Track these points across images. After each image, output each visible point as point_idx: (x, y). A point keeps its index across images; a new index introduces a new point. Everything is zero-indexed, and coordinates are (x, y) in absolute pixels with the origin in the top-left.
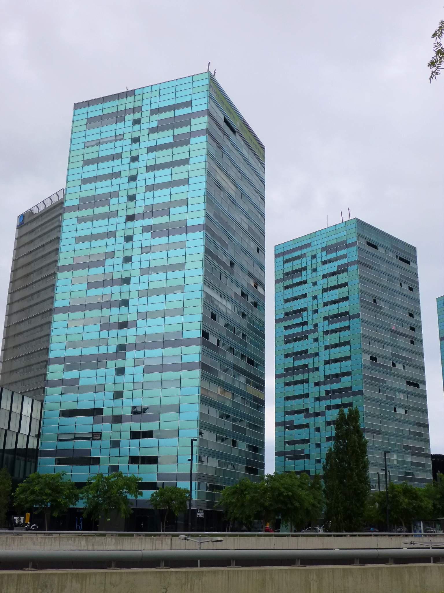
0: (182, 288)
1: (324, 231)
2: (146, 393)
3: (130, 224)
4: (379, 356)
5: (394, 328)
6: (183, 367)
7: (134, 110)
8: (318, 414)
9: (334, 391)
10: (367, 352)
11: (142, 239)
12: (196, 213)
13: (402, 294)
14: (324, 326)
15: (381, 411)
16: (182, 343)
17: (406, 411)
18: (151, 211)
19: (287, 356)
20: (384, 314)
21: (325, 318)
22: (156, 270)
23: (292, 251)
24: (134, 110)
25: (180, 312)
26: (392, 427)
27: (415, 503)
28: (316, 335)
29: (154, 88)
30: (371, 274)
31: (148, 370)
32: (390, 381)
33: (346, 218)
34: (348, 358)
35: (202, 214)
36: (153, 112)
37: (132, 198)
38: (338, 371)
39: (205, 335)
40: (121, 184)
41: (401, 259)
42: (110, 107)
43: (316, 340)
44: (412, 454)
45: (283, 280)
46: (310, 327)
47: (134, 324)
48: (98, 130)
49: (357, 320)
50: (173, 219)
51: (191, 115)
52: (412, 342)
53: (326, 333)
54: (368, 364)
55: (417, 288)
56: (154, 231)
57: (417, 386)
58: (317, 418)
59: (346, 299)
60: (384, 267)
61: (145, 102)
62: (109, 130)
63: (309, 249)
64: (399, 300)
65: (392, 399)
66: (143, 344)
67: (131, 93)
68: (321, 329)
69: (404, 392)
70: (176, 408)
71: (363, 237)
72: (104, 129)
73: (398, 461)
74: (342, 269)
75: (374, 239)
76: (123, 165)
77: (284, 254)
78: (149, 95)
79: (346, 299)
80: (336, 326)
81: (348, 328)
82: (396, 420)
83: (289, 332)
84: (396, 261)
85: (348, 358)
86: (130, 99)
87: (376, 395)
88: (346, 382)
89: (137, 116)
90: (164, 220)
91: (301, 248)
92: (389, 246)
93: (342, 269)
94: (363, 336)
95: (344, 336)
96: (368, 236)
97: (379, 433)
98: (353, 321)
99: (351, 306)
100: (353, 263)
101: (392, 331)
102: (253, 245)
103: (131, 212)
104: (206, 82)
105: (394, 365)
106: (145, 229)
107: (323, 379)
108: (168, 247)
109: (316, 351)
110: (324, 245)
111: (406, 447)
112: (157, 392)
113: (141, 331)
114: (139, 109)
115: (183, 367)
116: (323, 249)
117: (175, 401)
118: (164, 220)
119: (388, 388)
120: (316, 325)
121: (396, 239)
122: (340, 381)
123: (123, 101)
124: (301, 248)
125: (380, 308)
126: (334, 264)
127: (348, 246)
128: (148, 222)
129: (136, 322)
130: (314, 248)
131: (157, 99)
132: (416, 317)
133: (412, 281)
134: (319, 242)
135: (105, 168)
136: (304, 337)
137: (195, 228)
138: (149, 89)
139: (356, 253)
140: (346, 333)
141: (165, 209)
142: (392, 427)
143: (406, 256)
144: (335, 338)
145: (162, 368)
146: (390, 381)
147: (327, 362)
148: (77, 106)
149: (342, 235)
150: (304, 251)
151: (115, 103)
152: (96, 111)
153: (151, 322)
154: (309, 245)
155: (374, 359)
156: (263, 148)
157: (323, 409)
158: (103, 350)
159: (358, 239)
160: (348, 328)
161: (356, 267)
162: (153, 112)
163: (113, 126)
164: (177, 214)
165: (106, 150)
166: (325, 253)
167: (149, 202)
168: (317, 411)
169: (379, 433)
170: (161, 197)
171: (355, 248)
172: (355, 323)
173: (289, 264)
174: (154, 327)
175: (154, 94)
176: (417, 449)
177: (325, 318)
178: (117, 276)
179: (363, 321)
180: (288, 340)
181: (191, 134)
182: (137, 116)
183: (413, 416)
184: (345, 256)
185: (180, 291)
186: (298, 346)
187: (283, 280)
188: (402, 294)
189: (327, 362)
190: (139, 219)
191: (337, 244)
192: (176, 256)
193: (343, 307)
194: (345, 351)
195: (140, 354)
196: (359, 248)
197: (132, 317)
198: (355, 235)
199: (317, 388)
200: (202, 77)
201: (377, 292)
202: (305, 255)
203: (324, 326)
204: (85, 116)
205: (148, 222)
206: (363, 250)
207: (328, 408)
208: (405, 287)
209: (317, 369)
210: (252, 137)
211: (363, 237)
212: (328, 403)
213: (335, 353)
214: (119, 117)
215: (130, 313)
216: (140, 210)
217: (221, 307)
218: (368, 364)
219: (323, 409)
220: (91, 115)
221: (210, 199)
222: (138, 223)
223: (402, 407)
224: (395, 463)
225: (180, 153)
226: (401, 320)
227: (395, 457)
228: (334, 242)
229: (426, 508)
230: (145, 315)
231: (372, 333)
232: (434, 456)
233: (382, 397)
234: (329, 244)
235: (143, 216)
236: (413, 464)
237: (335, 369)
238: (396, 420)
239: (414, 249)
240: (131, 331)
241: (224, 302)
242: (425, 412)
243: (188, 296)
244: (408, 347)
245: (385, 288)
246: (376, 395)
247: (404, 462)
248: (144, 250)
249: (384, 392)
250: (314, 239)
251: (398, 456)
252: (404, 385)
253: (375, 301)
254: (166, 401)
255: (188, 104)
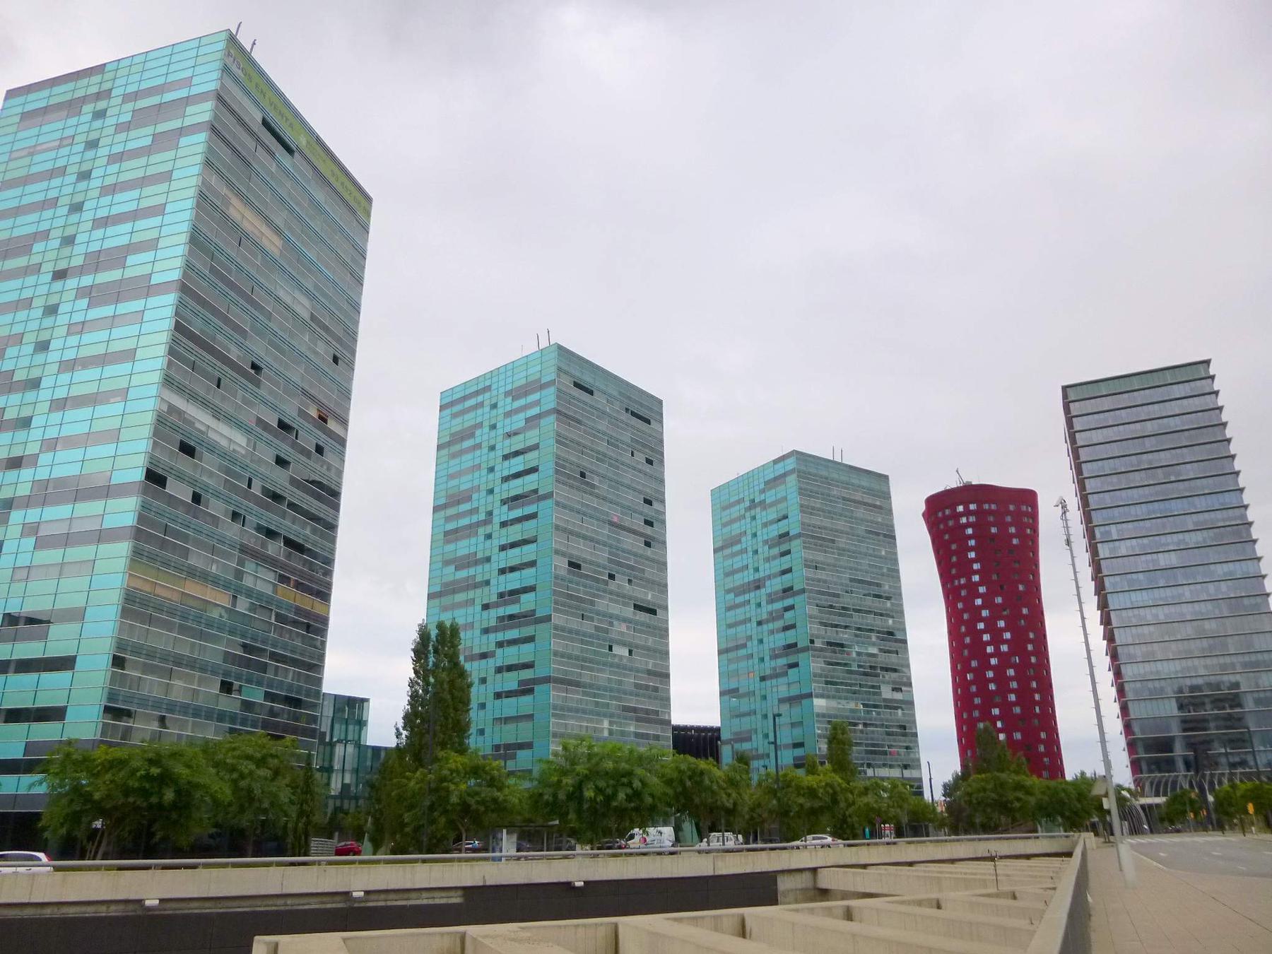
0: (123, 394)
1: (510, 367)
2: (33, 586)
3: (58, 285)
4: (585, 561)
5: (615, 520)
6: (103, 536)
7: (98, 96)
8: (484, 656)
9: (511, 617)
10: (564, 554)
11: (74, 309)
12: (169, 263)
13: (634, 469)
14: (502, 514)
15: (582, 650)
16: (107, 491)
17: (630, 652)
18: (96, 262)
19: (447, 563)
20: (597, 496)
21: (504, 502)
22: (86, 363)
23: (465, 398)
24: (98, 96)
25: (114, 436)
26: (604, 676)
27: (487, 793)
28: (488, 529)
29: (136, 60)
30: (573, 433)
31: (43, 543)
32: (603, 604)
33: (544, 344)
34: (532, 564)
35: (179, 263)
36: (127, 98)
37: (69, 241)
38: (517, 586)
39: (155, 478)
40: (55, 221)
41: (633, 414)
42: (62, 94)
43: (489, 536)
44: (638, 720)
45: (449, 444)
46: (482, 517)
47: (33, 460)
48: (35, 131)
49: (549, 502)
50: (129, 273)
51: (188, 101)
52: (648, 544)
53: (504, 524)
54: (563, 573)
55: (662, 462)
56: (94, 296)
57: (653, 612)
58: (484, 662)
59: (534, 470)
60: (603, 425)
61: (118, 82)
62: (53, 129)
63: (487, 395)
64: (628, 477)
65: (607, 631)
66: (46, 493)
67: (100, 69)
68: (496, 520)
69: (625, 620)
70: (77, 615)
71: (566, 373)
72: (45, 128)
73: (611, 732)
74: (532, 422)
75: (587, 379)
76: (64, 187)
77: (452, 404)
78: (126, 72)
79: (534, 470)
80: (517, 513)
81: (533, 516)
82: (612, 665)
83: (451, 526)
84: (625, 417)
85: (532, 564)
86: (96, 79)
87: (575, 623)
88: (527, 602)
89: (101, 105)
90: (115, 275)
91: (477, 393)
92: (615, 393)
93: (532, 422)
94: (557, 528)
95: (529, 528)
96: (578, 374)
97: (578, 684)
98: (542, 504)
99: (542, 481)
100: (547, 413)
101: (612, 524)
102: (321, 348)
103: (62, 265)
104: (222, 45)
105: (612, 577)
106: (81, 292)
107: (494, 598)
108: (113, 321)
109: (487, 554)
110: (509, 387)
111: (626, 709)
112: (51, 586)
113: (42, 474)
114: (107, 94)
115: (103, 536)
116: (507, 394)
117: (78, 601)
118: (115, 275)
119: (598, 613)
120: (490, 514)
121: (628, 384)
122: (518, 601)
123: (85, 81)
124: (477, 393)
125: (593, 486)
126: (522, 416)
127: (543, 387)
128: (87, 280)
129: (35, 457)
130: (494, 393)
131: (137, 77)
132: (656, 505)
133: (652, 450)
134: (502, 383)
135: (35, 193)
136: (472, 529)
137: (162, 288)
138: (127, 62)
139: (553, 397)
140: (531, 524)
141: (117, 257)
142: (604, 676)
143: (644, 412)
144: (515, 533)
145: (67, 540)
146: (603, 604)
147: (502, 571)
148: (11, 94)
149: (534, 370)
150: (480, 399)
151: (71, 86)
152: (37, 101)
153: (62, 455)
154: (487, 389)
155: (574, 565)
156: (369, 200)
157: (492, 647)
158: (475, 519)
159: (559, 376)
160: (533, 516)
161: (552, 418)
162: (127, 98)
163: (60, 125)
164: (137, 264)
165: (43, 163)
166: (509, 400)
167: (95, 247)
168: (484, 650)
169: (578, 684)
170: (118, 236)
171: (552, 390)
172: (545, 508)
173: (459, 420)
174: (65, 465)
175: (134, 69)
176: (647, 712)
177: (504, 502)
178: (480, 555)
179: (558, 504)
180: (451, 536)
181: (182, 132)
182: (101, 105)
183: (641, 661)
184: (537, 403)
185: (119, 399)
186: (463, 548)
187: (449, 444)
188: (634, 469)
189: (502, 571)
190: (73, 276)
191: (527, 385)
192: (122, 338)
193: (529, 482)
194: (528, 552)
195: (33, 515)
196: (559, 390)
197: (32, 449)
198: (553, 369)
199: (485, 613)
200: (216, 38)
201: (587, 462)
202: (481, 404)
203: (502, 514)
204: (19, 110)
205: (87, 280)
206: (565, 393)
207: (500, 644)
208: (639, 457)
209: (487, 583)
210: (337, 171)
211: (566, 373)
212: (500, 636)
213: (514, 556)
214: (72, 107)
215: (30, 442)
216: (78, 261)
217: (212, 435)
218: (563, 573)
219: (492, 647)
220: (29, 107)
221: (196, 240)
222: (71, 283)
223: (624, 644)
224: (606, 734)
225: (160, 162)
226: (629, 508)
227: (606, 724)
228: (523, 382)
229: (505, 801)
230: (51, 445)
231: (574, 522)
232: (676, 728)
233: (588, 627)
234: (517, 384)
235: (81, 271)
236: (637, 735)
237: (513, 581)
238: (612, 665)
239: (660, 402)
240: (26, 474)
241: (224, 429)
242: (666, 654)
243: (131, 406)
244: (641, 552)
245: (601, 457)
246: (575, 623)
247: (623, 733)
248: (73, 329)
249: (592, 619)
250: (495, 379)
251: (611, 723)
252: (629, 611)
253: (583, 475)
254: (64, 603)
255: (188, 82)
